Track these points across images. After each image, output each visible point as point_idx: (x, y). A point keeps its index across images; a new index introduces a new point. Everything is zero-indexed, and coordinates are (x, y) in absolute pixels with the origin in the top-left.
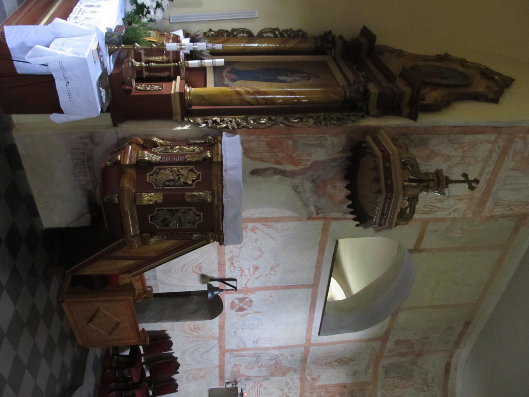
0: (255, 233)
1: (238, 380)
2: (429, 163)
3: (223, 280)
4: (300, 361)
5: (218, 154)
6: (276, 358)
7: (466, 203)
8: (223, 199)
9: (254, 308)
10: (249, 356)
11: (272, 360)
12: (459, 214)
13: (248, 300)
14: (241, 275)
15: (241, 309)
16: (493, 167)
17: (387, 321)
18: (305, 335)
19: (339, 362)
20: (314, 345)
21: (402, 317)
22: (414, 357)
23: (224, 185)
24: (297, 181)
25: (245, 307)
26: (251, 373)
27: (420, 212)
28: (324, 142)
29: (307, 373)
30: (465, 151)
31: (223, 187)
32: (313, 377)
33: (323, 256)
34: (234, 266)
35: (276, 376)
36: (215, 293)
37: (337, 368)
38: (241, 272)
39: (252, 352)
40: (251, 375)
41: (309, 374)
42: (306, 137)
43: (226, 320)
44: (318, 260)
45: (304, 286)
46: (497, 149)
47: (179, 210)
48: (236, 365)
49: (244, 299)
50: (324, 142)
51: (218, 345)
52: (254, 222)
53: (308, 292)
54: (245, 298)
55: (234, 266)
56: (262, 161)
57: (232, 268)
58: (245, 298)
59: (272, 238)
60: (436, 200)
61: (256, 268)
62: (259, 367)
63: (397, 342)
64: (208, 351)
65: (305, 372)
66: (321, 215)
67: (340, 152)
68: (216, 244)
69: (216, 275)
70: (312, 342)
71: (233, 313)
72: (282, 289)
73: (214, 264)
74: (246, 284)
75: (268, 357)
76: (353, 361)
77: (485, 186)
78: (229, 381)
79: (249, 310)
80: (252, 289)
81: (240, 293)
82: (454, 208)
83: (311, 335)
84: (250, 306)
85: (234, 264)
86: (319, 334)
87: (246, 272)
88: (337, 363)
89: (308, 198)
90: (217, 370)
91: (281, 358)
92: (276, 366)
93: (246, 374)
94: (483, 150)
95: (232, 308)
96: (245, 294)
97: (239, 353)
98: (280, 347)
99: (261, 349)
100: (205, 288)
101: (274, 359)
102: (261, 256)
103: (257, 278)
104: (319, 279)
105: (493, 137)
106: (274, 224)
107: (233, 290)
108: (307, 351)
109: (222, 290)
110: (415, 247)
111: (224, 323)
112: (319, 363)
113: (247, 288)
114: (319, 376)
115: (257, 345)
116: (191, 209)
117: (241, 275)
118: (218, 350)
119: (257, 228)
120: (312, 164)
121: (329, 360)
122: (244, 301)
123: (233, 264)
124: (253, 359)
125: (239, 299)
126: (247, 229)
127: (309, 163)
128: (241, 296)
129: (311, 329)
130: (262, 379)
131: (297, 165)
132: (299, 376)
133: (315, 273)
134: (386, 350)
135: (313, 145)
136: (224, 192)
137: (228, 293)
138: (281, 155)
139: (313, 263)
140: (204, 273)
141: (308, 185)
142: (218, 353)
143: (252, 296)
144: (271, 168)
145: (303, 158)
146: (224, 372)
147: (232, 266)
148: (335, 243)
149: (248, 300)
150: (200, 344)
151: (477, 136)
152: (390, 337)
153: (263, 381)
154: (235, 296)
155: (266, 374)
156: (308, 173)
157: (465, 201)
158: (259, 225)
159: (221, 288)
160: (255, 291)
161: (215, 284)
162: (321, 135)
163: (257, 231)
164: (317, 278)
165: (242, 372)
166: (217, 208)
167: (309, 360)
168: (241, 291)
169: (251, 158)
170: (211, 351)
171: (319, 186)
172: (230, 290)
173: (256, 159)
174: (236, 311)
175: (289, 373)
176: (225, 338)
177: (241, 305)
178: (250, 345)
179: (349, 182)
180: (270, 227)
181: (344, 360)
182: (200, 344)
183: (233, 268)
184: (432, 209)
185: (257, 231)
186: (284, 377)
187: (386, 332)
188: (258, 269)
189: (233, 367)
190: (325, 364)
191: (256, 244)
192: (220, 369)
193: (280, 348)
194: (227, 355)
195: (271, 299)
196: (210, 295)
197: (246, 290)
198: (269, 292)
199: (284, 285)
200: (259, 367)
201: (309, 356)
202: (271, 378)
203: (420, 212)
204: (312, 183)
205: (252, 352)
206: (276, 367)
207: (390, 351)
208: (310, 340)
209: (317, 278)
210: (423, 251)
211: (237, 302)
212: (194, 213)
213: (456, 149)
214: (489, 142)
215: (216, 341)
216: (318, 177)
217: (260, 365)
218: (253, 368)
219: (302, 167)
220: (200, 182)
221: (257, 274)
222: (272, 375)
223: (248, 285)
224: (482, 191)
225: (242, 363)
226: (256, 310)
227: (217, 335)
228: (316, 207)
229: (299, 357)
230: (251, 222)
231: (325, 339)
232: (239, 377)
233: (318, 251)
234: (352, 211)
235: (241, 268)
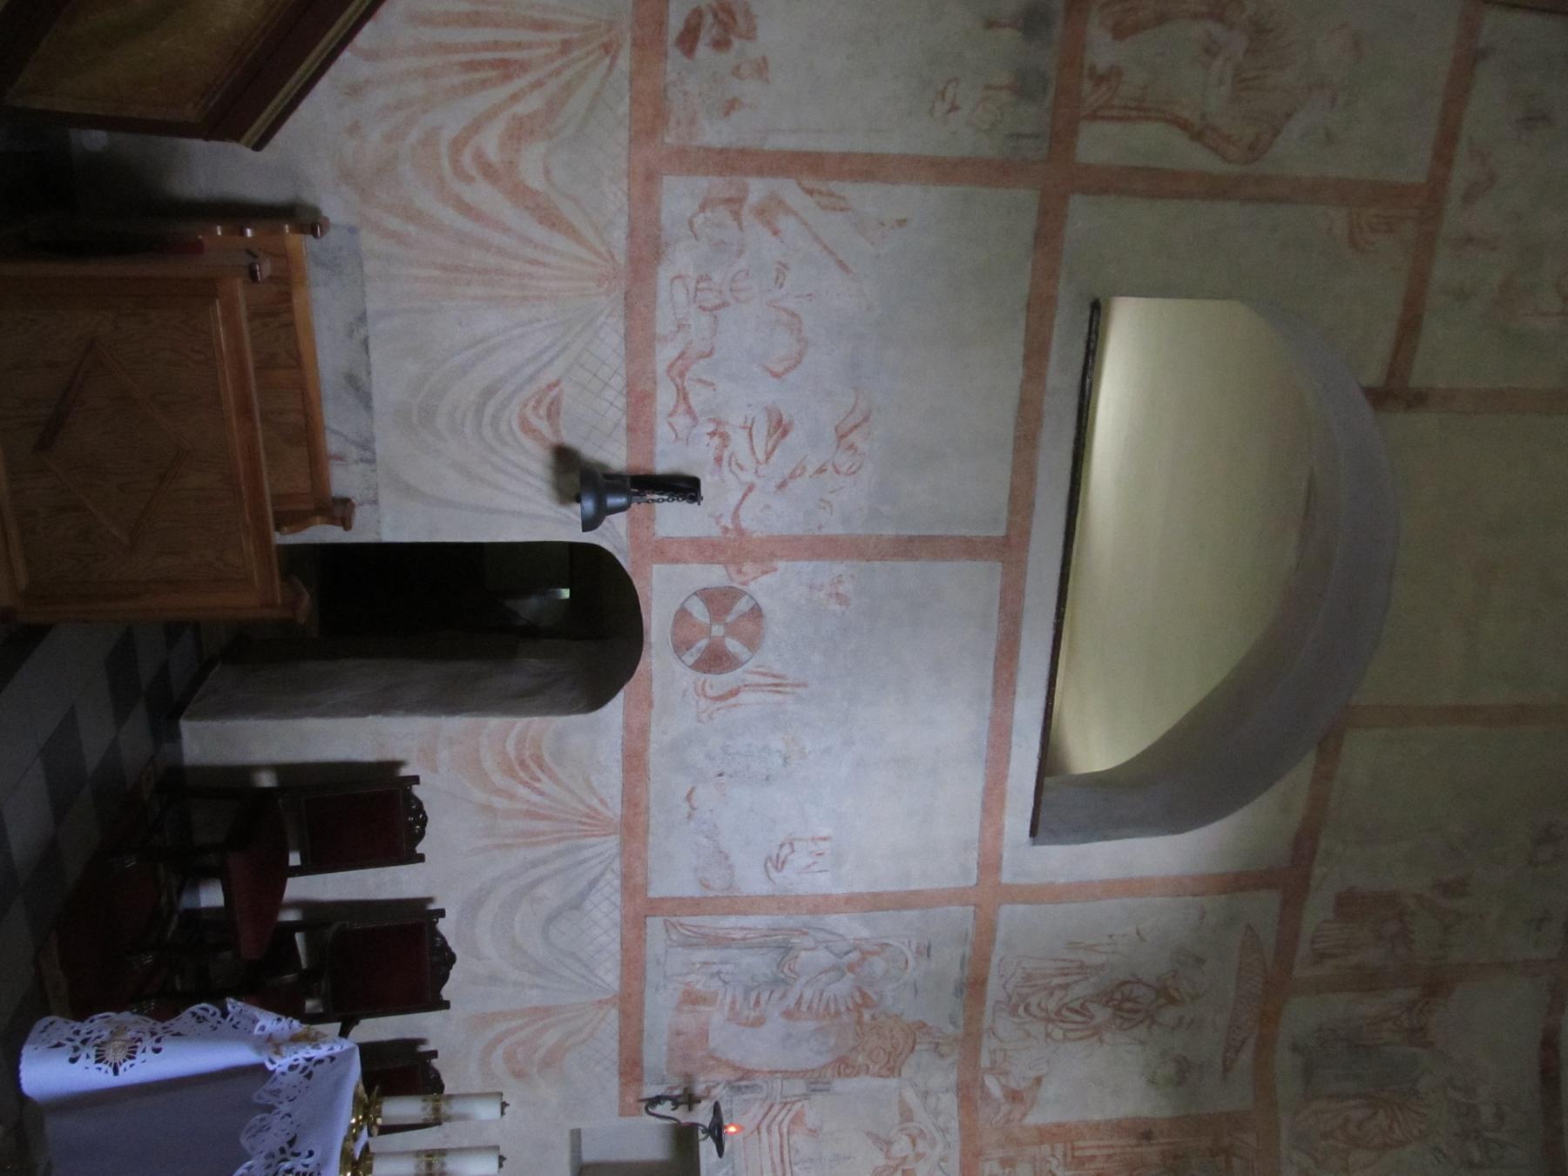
63: (1349, 905)
76: (1172, 1001)
110: (1391, 374)
134: (1303, 949)
152: (1318, 871)
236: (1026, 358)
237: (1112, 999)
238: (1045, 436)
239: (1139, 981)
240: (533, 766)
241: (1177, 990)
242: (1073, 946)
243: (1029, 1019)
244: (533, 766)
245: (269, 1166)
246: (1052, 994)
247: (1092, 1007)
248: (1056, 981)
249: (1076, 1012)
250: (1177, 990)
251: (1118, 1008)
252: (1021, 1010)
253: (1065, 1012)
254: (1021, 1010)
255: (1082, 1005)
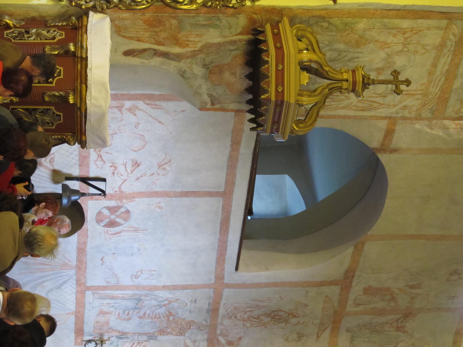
0: (135, 115)
1: (105, 338)
2: (359, 50)
3: (85, 180)
4: (208, 311)
5: (82, 47)
6: (168, 304)
7: (418, 99)
8: (87, 101)
9: (132, 222)
10: (124, 299)
11: (160, 306)
12: (410, 113)
13: (123, 210)
14: (113, 173)
15: (112, 224)
16: (450, 57)
18: (214, 269)
19: (273, 318)
20: (228, 286)
21: (372, 250)
22: (398, 316)
23: (88, 86)
24: (183, 65)
25: (118, 220)
26: (128, 327)
27: (354, 108)
28: (218, 23)
29: (218, 332)
30: (408, 38)
31: (87, 87)
32: (229, 339)
34: (102, 160)
35: (168, 334)
36: (74, 198)
37: (268, 326)
38: (113, 168)
39: (130, 292)
40: (127, 330)
41: (222, 334)
42: (194, 17)
43: (89, 239)
44: (230, 157)
45: (210, 194)
46: (452, 37)
47: (37, 109)
48: (102, 313)
49: (117, 208)
50: (218, 23)
51: (74, 277)
52: (133, 99)
53: (216, 204)
54: (119, 207)
55: (102, 160)
56: (139, 40)
57: (99, 163)
58: (119, 207)
59: (160, 122)
60: (375, 94)
61: (136, 164)
62: (140, 317)
64: (59, 287)
65: (215, 329)
66: (217, 106)
67: (241, 34)
68: (77, 146)
69: (76, 172)
70: (226, 281)
71: (100, 228)
72: (176, 196)
73: (72, 156)
74: (120, 187)
75: (154, 302)
76: (295, 316)
77: (443, 79)
78: (90, 338)
79: (126, 226)
80: (130, 194)
81: (111, 199)
82: (403, 104)
83: (223, 269)
84: (126, 220)
85: (103, 158)
86: (237, 269)
87: (121, 169)
88: (269, 319)
89: (200, 85)
90: (72, 319)
91: (176, 305)
92: (168, 316)
93: (119, 328)
94: (432, 38)
95: (98, 221)
96: (118, 202)
97: (109, 292)
98: (174, 286)
99: (144, 288)
100: (58, 189)
101: (165, 305)
102: (144, 147)
103: (138, 179)
104: (233, 184)
105: (444, 23)
106: (163, 104)
107: (100, 195)
108: (218, 296)
109: (83, 194)
110: (383, 144)
111: (85, 243)
112: (238, 317)
113: (122, 192)
114: (240, 338)
115: (137, 281)
116: (50, 109)
117: (113, 173)
118: (75, 286)
119: (137, 108)
120: (202, 46)
121: (256, 313)
122: (117, 211)
123: (101, 157)
124: (130, 304)
125: (109, 208)
126: (123, 109)
127: (199, 46)
128: (112, 203)
129: (224, 260)
130: (145, 338)
131: (184, 47)
132: (206, 336)
133: (227, 174)
134: (350, 302)
135: (204, 25)
136: (88, 93)
137: (92, 199)
138: (163, 35)
139: (223, 160)
140: (57, 167)
141: (198, 70)
142: (74, 291)
143: (129, 205)
144: (150, 49)
145: (191, 39)
146: (83, 322)
147: (100, 159)
149: (123, 210)
150: (47, 276)
151: (420, 21)
153: (147, 341)
154: (103, 203)
155: (151, 331)
156: (198, 56)
157: (416, 97)
158: (140, 104)
159: (82, 191)
160: (134, 197)
161: (74, 185)
162: (213, 15)
163: (137, 112)
164: (230, 183)
165: (112, 324)
166: (80, 108)
167: (222, 311)
168: (113, 197)
169: (124, 37)
170: (63, 287)
171: (213, 71)
172: (96, 195)
173: (131, 38)
174: (105, 226)
175: (189, 331)
176: (86, 268)
177: (113, 217)
178: (126, 280)
179: (251, 70)
180: (160, 108)
181: (281, 313)
182: (47, 276)
183: (102, 162)
184: (371, 105)
185: (137, 112)
186: (182, 338)
188: (138, 166)
189: (98, 315)
190: (248, 318)
191: (136, 130)
192: (77, 317)
193: (174, 288)
194: (89, 294)
195: (159, 210)
196: (65, 201)
197: (120, 196)
198: (155, 200)
199: (179, 190)
200: (140, 317)
201: (222, 304)
202: (160, 338)
203: (354, 108)
204: (203, 67)
205: (130, 292)
206: (168, 320)
208: (223, 278)
209: (230, 183)
210: (395, 150)
211: (106, 212)
212: (54, 113)
213: (394, 36)
214: (440, 28)
215: (72, 272)
216: (212, 62)
217: (141, 314)
218: (129, 319)
219: (189, 49)
220: (61, 79)
221: (137, 173)
222: (162, 332)
223: (123, 188)
224: (439, 86)
225: (112, 309)
226: (135, 226)
227: (74, 262)
228: (210, 96)
229: (204, 304)
230: (129, 99)
231: (247, 275)
232: (108, 332)
233: (230, 143)
234: (251, 109)
235: (113, 163)
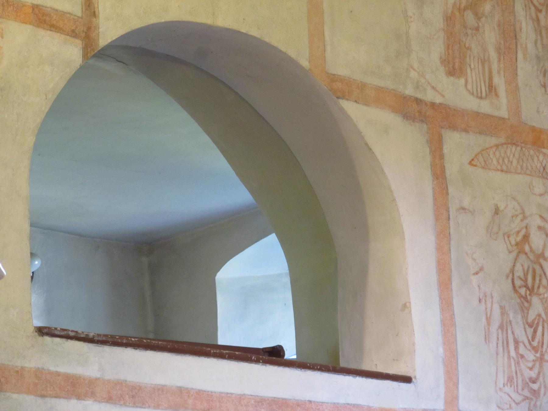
17: (530, 288)
33: (92, 383)
63: (454, 67)
76: (526, 238)
86: (407, 380)
110: (74, 34)
134: (485, 107)
148: (47, 339)
152: (430, 96)
181: (519, 272)
187: (407, 116)
207: (492, 89)
231: (424, 355)
236: (79, 397)
237: (525, 298)
238: (132, 377)
239: (512, 271)
240: (472, 58)
241: (518, 232)
242: (487, 338)
243: (541, 379)
244: (472, 58)
245: (8, 16)
246: (522, 356)
247: (531, 317)
248: (513, 353)
249: (535, 332)
250: (518, 232)
251: (531, 290)
252: (535, 386)
253: (535, 344)
254: (535, 386)
255: (531, 326)
